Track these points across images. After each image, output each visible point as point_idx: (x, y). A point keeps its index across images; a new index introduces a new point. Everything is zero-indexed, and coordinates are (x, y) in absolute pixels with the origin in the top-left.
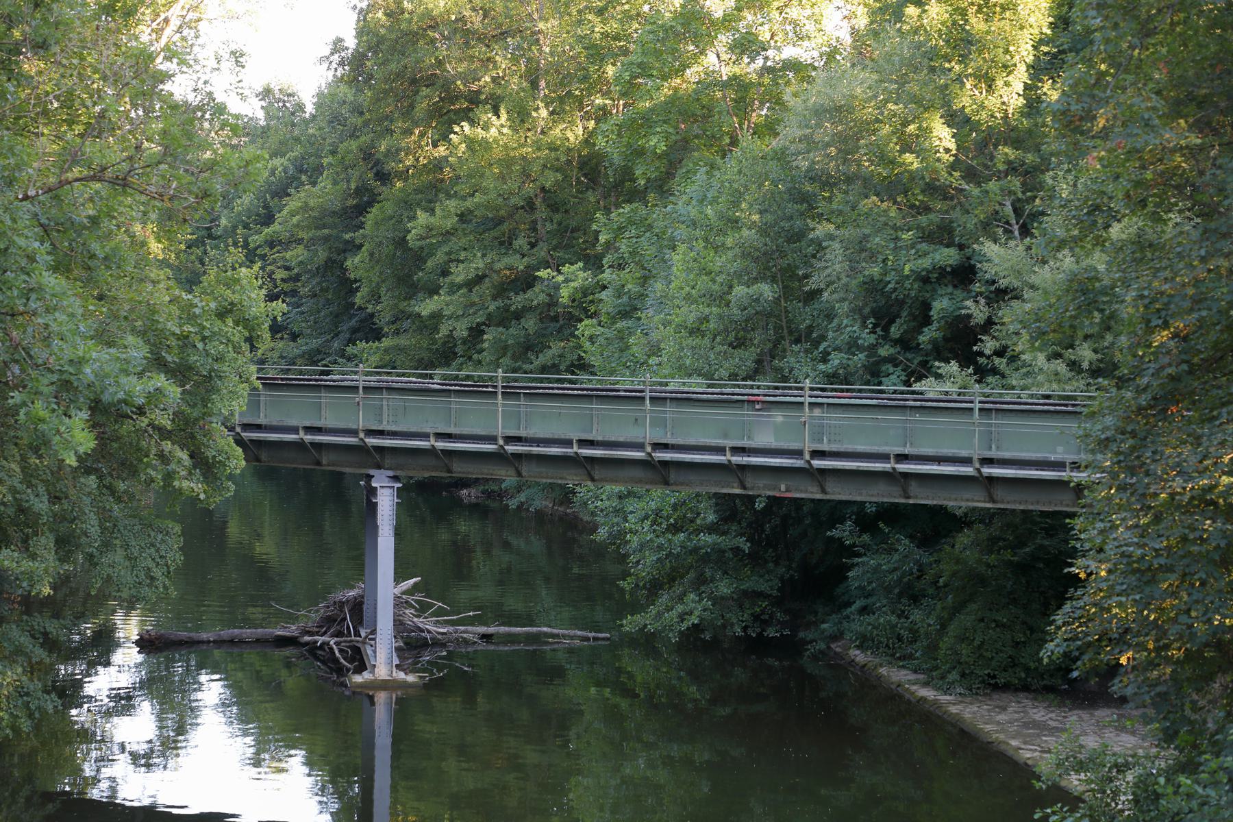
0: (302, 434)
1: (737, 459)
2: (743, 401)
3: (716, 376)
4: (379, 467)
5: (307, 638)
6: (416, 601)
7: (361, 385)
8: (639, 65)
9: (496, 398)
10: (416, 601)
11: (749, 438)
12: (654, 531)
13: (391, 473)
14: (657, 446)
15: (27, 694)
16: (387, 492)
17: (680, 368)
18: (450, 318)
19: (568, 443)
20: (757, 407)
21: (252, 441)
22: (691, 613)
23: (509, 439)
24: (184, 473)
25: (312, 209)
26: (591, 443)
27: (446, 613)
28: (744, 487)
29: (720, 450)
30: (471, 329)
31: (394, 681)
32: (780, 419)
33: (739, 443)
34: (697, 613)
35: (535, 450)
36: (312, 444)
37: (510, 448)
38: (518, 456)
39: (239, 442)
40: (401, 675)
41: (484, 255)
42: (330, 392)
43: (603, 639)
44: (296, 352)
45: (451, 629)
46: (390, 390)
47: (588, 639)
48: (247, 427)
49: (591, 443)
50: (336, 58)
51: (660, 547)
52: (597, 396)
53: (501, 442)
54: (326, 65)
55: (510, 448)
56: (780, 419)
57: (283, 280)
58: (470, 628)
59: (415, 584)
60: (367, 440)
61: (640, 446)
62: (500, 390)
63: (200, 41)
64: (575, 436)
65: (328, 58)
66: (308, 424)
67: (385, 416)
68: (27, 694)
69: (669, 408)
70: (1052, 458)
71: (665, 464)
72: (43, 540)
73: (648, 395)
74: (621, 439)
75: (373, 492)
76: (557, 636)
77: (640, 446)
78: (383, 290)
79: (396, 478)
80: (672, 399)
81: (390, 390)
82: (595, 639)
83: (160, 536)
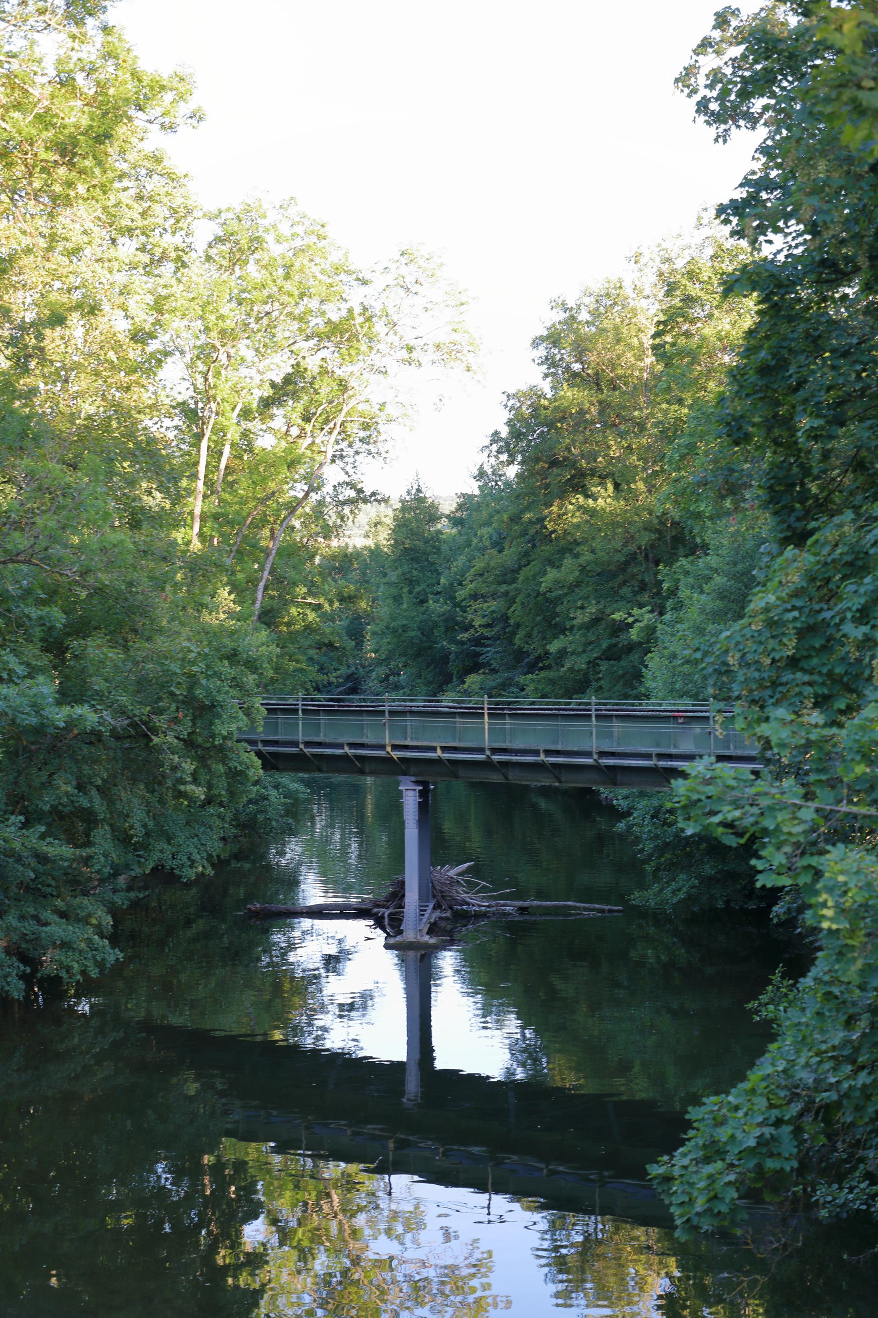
0: (347, 749)
1: (662, 763)
2: (669, 717)
3: (701, 697)
4: (405, 774)
5: (375, 910)
6: (465, 881)
7: (387, 709)
8: (686, 446)
9: (591, 721)
10: (465, 881)
11: (675, 747)
12: (654, 824)
13: (413, 779)
14: (602, 754)
15: (96, 949)
16: (411, 793)
17: (672, 691)
18: (573, 653)
19: (536, 753)
20: (680, 721)
21: (270, 753)
22: (679, 890)
23: (495, 751)
24: (189, 779)
25: (494, 568)
26: (557, 753)
27: (491, 891)
28: (560, 782)
29: (648, 756)
30: (589, 663)
31: (418, 942)
32: (698, 730)
33: (552, 747)
34: (685, 889)
35: (514, 758)
36: (448, 760)
37: (496, 758)
38: (502, 764)
39: (259, 754)
40: (426, 938)
41: (598, 602)
42: (622, 722)
43: (617, 911)
44: (493, 684)
45: (493, 903)
46: (412, 713)
47: (603, 911)
48: (266, 743)
49: (557, 753)
50: (495, 447)
51: (656, 837)
52: (562, 715)
53: (488, 753)
54: (486, 453)
55: (496, 758)
56: (698, 730)
57: (480, 626)
58: (509, 902)
59: (469, 867)
60: (493, 757)
61: (588, 754)
62: (486, 712)
63: (381, 438)
64: (541, 747)
65: (487, 447)
66: (351, 740)
67: (409, 733)
68: (96, 949)
69: (616, 724)
70: (317, 739)
71: (609, 768)
72: (101, 831)
73: (593, 713)
74: (575, 749)
75: (400, 794)
76: (579, 908)
77: (588, 754)
78: (535, 632)
79: (417, 783)
80: (617, 716)
81: (412, 713)
82: (610, 911)
83: (203, 829)
